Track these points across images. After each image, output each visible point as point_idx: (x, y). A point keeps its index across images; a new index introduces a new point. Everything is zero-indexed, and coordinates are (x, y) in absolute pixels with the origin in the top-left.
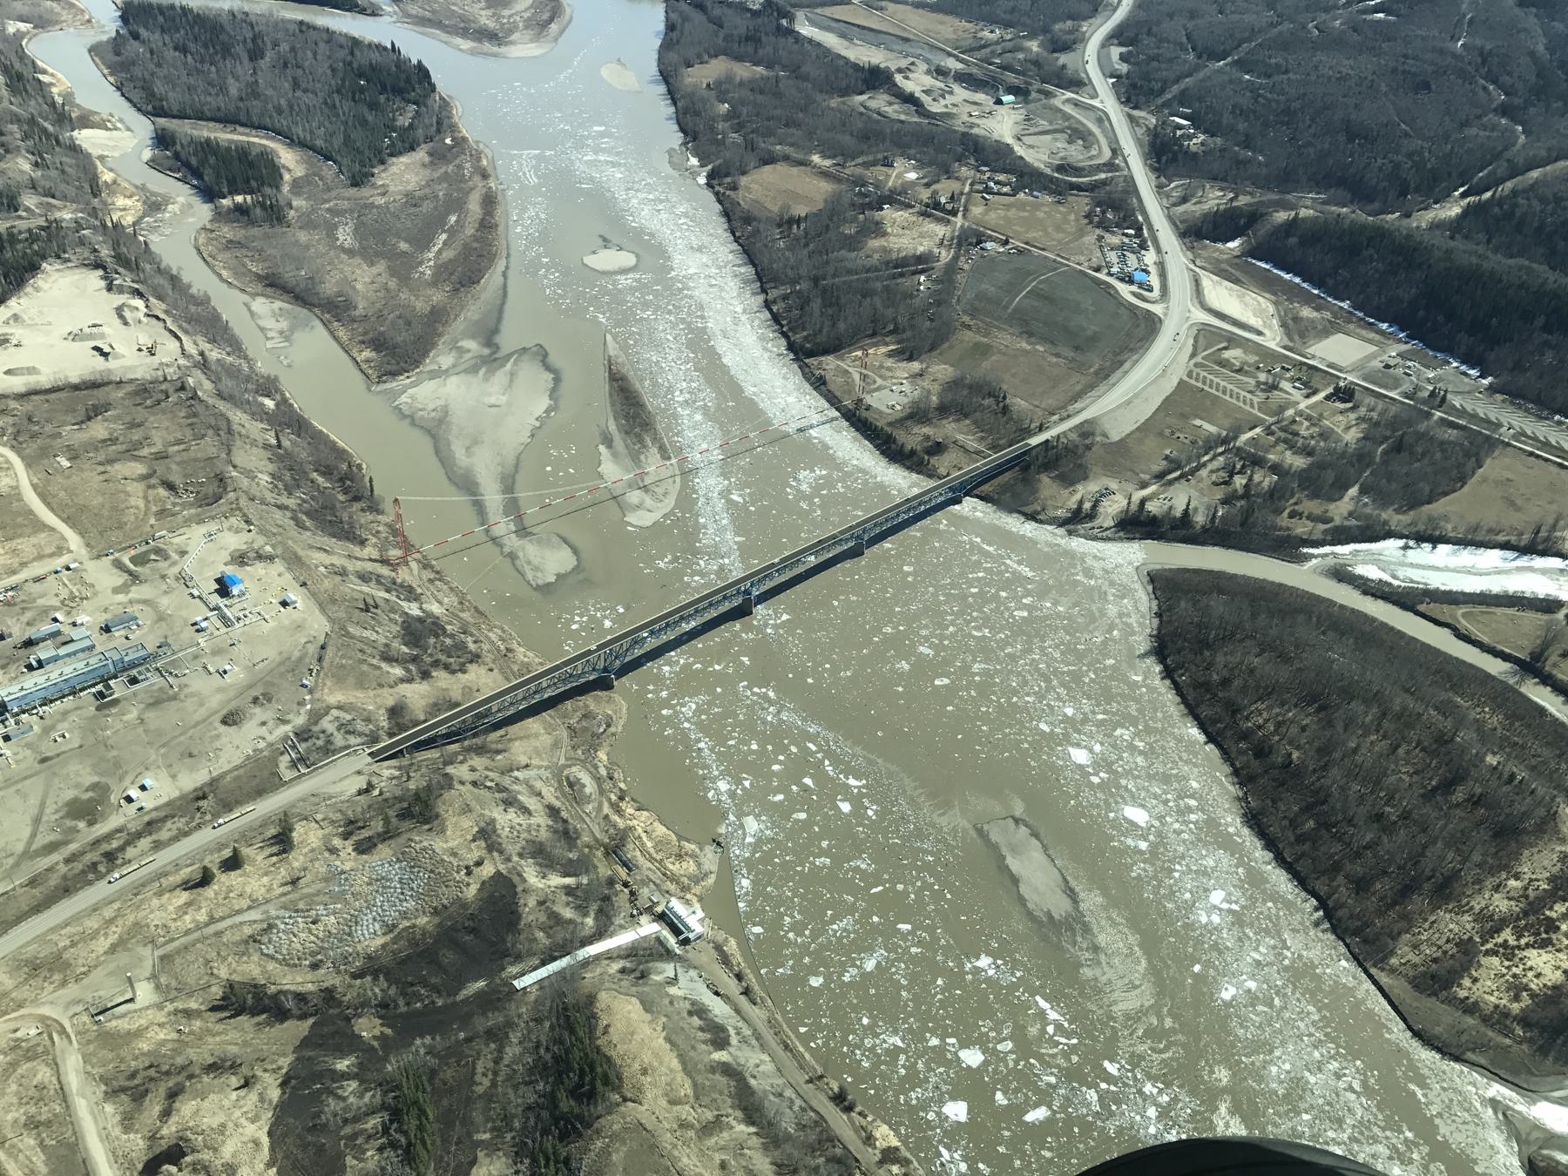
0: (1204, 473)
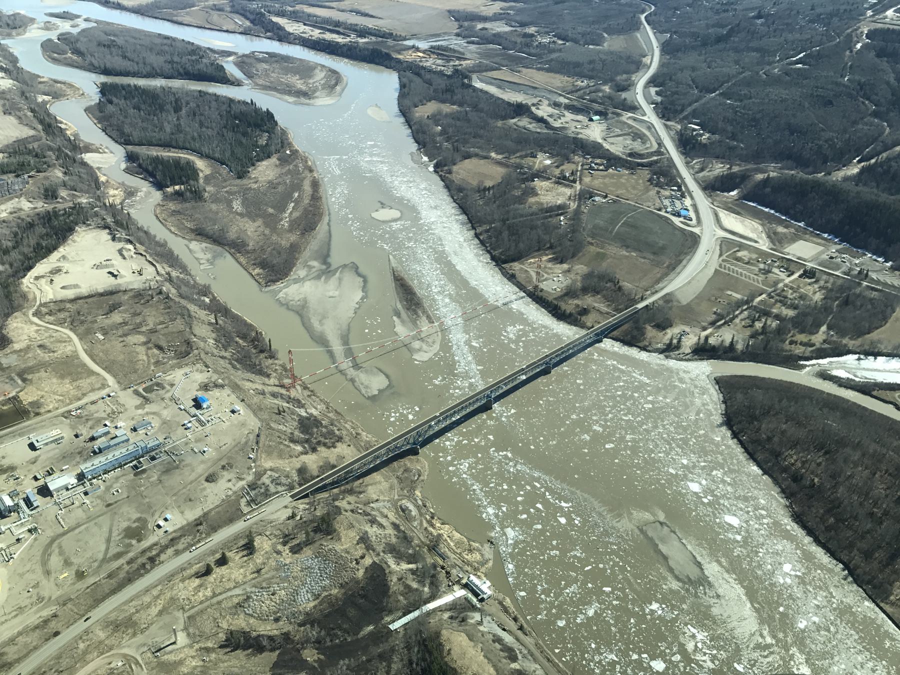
0: (737, 321)
